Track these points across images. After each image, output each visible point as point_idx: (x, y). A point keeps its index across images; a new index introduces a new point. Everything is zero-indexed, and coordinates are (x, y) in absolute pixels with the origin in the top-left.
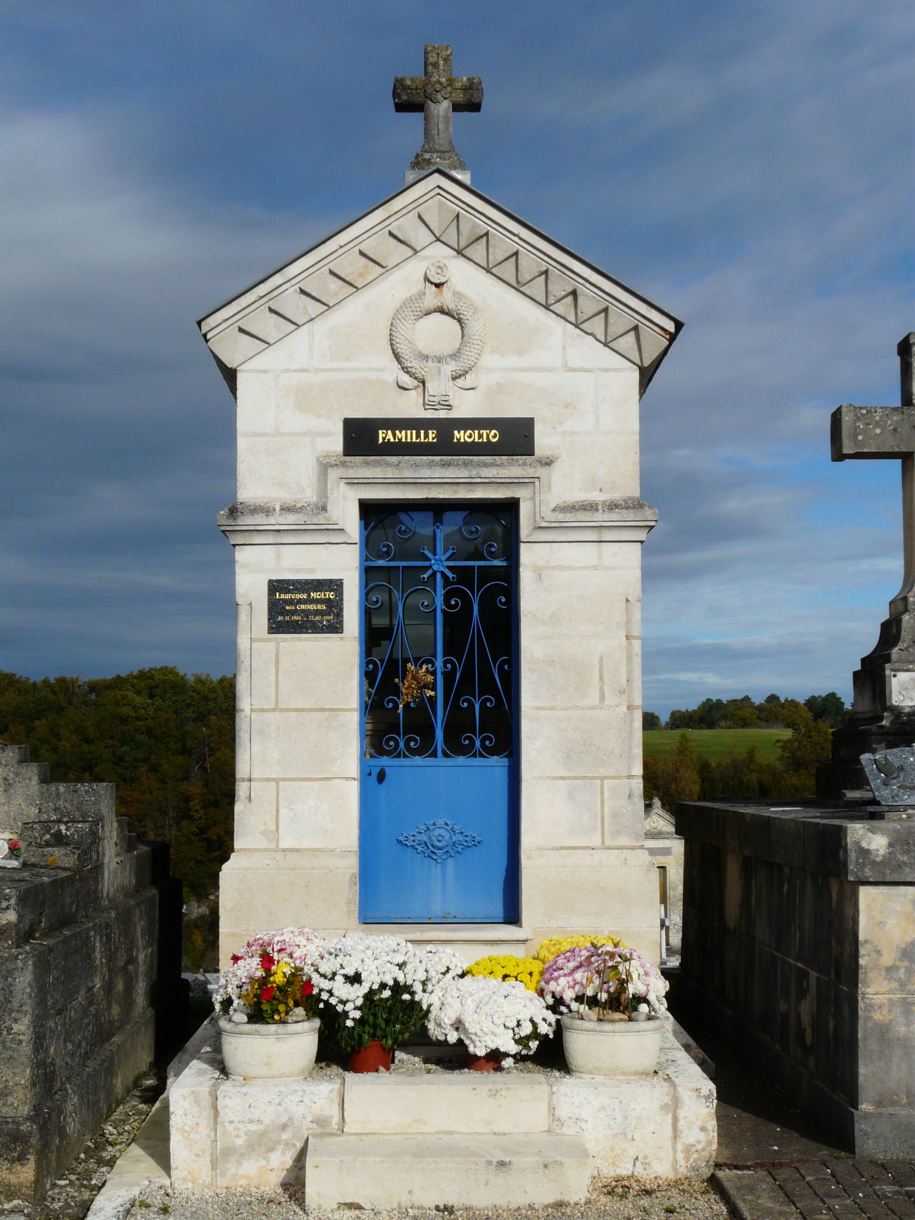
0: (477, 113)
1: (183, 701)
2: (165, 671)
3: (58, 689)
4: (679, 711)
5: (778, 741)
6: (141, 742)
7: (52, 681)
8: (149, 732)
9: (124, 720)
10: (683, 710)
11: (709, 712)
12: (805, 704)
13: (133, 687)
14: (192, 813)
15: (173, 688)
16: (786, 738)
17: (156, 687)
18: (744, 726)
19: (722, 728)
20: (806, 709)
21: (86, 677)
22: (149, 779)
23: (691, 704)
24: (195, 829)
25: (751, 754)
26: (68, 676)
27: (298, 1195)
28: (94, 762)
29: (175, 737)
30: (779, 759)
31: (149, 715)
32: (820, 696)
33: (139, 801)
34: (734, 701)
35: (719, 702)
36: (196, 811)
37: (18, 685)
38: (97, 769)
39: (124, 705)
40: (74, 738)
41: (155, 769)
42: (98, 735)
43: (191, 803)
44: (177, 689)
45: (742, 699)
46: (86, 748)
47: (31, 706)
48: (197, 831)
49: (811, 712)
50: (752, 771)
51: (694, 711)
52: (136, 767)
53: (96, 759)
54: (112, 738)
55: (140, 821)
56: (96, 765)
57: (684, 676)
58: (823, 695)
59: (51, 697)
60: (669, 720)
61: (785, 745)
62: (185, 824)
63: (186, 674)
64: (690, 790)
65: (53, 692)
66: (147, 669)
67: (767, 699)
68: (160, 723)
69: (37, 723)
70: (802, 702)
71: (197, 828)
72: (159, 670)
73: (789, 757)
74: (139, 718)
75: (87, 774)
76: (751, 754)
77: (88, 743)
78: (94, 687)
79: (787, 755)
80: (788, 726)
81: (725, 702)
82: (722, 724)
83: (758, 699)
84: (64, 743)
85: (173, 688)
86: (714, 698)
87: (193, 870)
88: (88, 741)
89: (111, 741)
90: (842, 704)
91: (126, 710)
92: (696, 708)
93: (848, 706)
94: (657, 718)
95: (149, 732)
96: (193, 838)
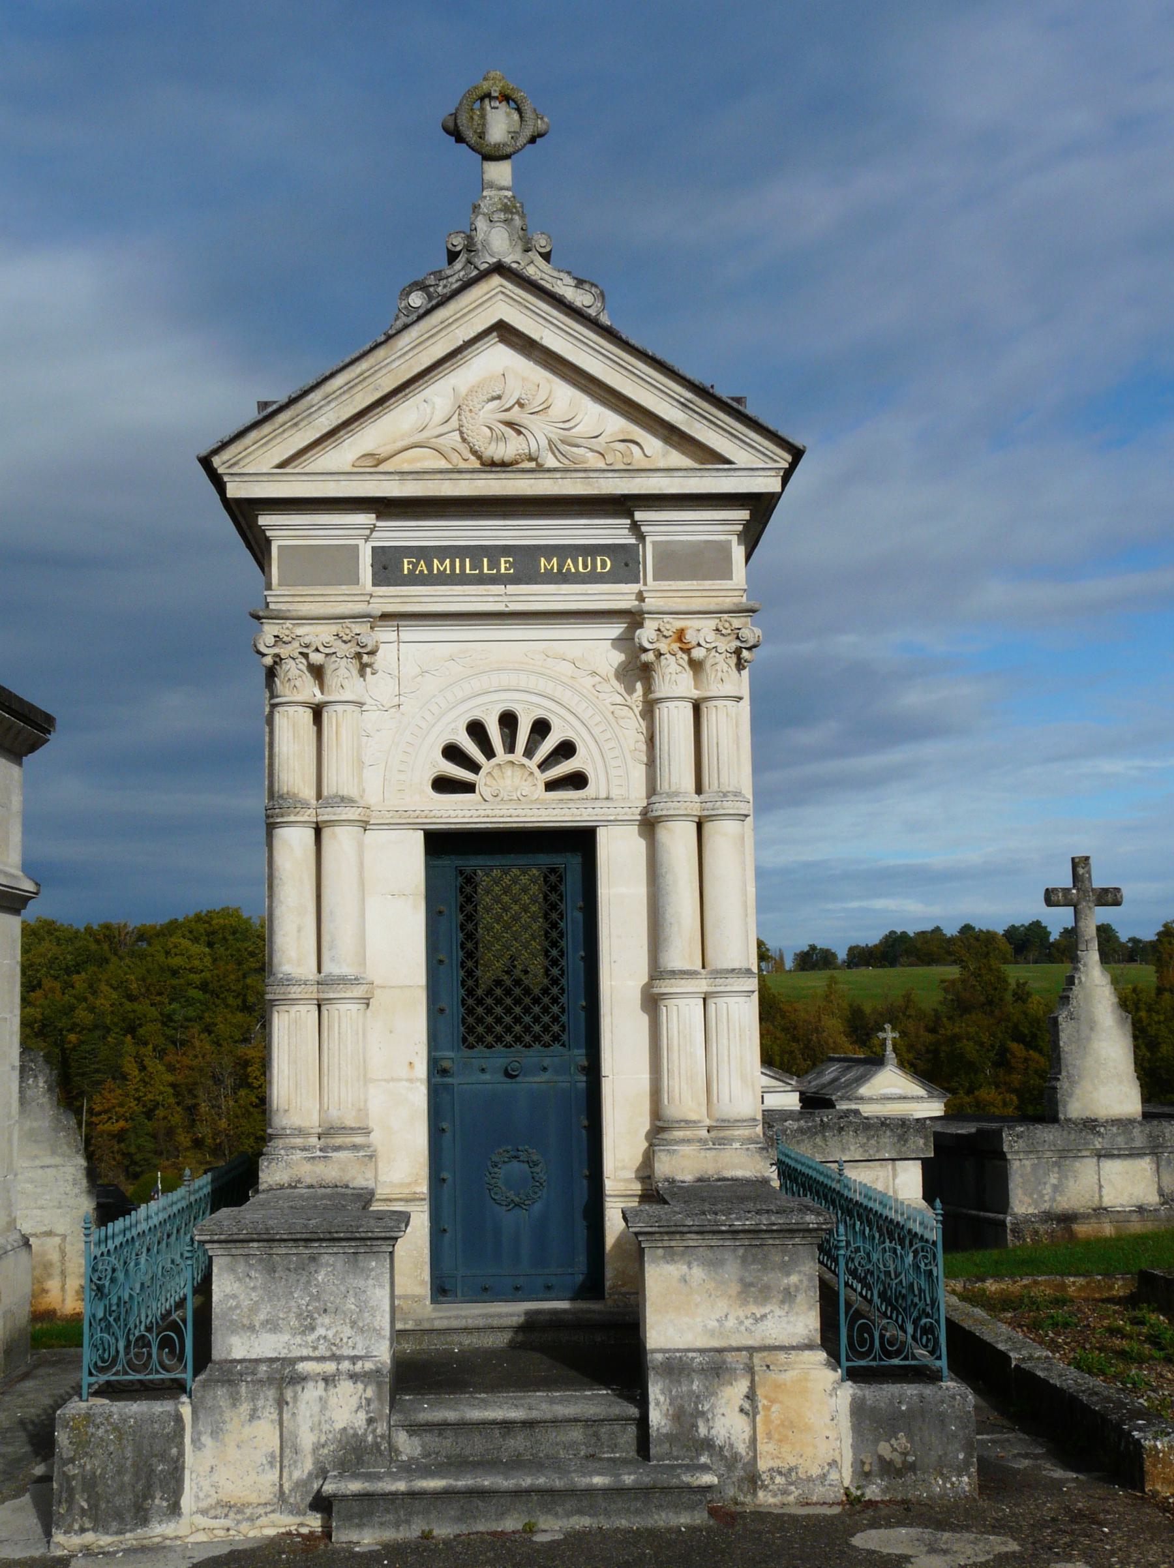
0: (506, 320)
1: (246, 950)
2: (225, 912)
3: (101, 937)
4: (857, 947)
5: (942, 981)
6: (193, 999)
7: (95, 927)
8: (204, 987)
9: (175, 973)
10: (863, 945)
11: (893, 946)
12: (1003, 935)
13: (191, 932)
14: (250, 1080)
15: (234, 933)
16: (951, 977)
17: (213, 933)
18: (930, 962)
19: (903, 966)
20: (1004, 940)
21: (134, 923)
22: (201, 1041)
23: (872, 937)
24: (254, 1099)
25: (908, 998)
26: (114, 921)
27: (173, 1485)
28: (138, 1022)
29: (234, 991)
30: (941, 1003)
31: (206, 967)
32: (1023, 925)
33: (191, 1068)
34: (923, 932)
35: (904, 934)
36: (255, 1078)
37: (57, 933)
38: (141, 1031)
39: (176, 955)
40: (115, 996)
41: (208, 1030)
42: (143, 990)
43: (250, 1069)
44: (238, 935)
45: (933, 931)
46: (128, 1006)
47: (69, 957)
48: (257, 1101)
49: (1011, 944)
50: (909, 1016)
51: (876, 946)
52: (187, 1028)
53: (139, 1019)
54: (160, 994)
55: (190, 1091)
56: (141, 1025)
57: (880, 904)
58: (1027, 924)
59: (93, 947)
60: (846, 957)
61: (948, 986)
62: (242, 1092)
63: (250, 918)
64: (834, 1043)
65: (97, 941)
66: (205, 912)
67: (961, 929)
68: (218, 976)
69: (75, 977)
70: (1002, 932)
71: (257, 1097)
72: (218, 913)
73: (952, 1000)
74: (192, 970)
75: (129, 1037)
76: (908, 998)
77: (131, 1001)
78: (142, 935)
79: (950, 997)
80: (955, 962)
81: (912, 935)
82: (903, 960)
83: (951, 930)
84: (103, 1001)
85: (234, 933)
86: (899, 931)
87: (252, 1147)
88: (131, 998)
89: (158, 998)
90: (1048, 934)
91: (176, 961)
92: (877, 942)
93: (1052, 939)
94: (834, 955)
95: (204, 987)
96: (252, 1109)
